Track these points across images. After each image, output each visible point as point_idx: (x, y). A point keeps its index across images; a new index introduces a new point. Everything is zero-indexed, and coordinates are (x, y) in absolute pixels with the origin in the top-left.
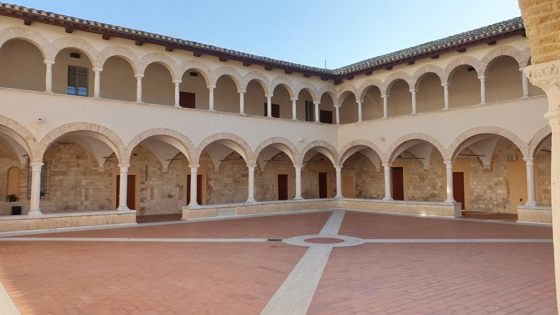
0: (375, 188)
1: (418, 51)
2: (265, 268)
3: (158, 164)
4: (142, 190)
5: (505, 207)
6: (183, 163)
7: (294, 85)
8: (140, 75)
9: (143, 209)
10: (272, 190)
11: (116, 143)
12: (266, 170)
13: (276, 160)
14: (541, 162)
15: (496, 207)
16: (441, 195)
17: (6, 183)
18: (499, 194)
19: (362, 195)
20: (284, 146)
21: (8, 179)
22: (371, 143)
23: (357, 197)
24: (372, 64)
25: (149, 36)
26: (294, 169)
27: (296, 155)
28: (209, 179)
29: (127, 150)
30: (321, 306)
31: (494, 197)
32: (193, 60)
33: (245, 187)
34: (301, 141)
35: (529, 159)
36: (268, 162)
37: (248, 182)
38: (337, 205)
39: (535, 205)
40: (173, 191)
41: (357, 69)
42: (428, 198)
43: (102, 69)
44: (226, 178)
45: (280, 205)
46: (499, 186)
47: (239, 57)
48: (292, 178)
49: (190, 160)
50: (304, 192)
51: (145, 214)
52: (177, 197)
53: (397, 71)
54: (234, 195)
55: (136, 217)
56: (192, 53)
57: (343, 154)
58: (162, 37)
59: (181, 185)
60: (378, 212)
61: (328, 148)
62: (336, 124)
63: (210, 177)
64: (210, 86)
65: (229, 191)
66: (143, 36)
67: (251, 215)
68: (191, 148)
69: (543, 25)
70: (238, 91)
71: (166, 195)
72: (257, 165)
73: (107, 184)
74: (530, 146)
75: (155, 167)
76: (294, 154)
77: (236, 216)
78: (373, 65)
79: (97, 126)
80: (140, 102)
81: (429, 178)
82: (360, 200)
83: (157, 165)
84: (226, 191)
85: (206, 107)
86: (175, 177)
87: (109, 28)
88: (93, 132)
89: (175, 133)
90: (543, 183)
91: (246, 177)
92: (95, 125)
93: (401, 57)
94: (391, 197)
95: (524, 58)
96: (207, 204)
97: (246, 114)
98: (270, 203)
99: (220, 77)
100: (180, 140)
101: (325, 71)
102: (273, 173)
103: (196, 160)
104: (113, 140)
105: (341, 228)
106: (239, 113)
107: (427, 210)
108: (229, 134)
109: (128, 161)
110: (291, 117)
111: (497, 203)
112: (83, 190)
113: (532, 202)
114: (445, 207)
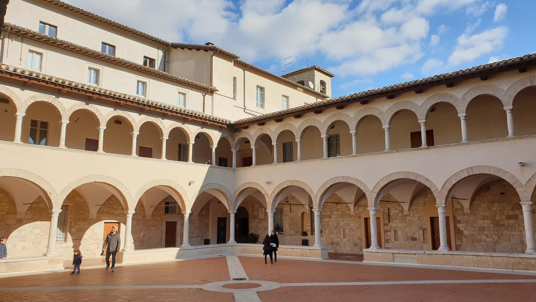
4: (386, 231)
28: (456, 222)
32: (365, 109)
40: (416, 233)
45: (484, 259)
59: (424, 228)
63: (458, 219)
71: (410, 237)
73: (358, 225)
79: (297, 181)
83: (398, 208)
84: (482, 236)
96: (457, 249)
98: (463, 254)
112: (342, 230)
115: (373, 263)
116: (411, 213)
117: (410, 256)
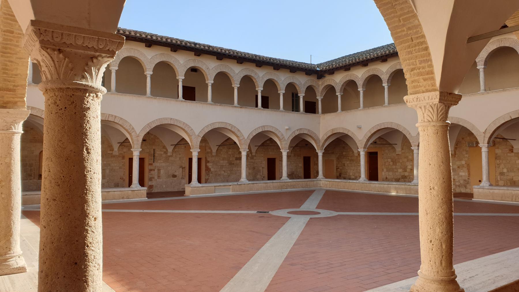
0: (353, 170)
1: (390, 50)
2: (254, 232)
3: (164, 148)
4: (151, 170)
5: (466, 187)
6: (185, 147)
7: (281, 80)
8: (149, 73)
9: (151, 187)
10: (262, 172)
11: (129, 131)
12: (257, 154)
13: (265, 146)
14: (498, 148)
15: (458, 187)
16: (410, 177)
17: (38, 164)
18: (461, 176)
19: (342, 176)
20: (271, 133)
21: (39, 161)
22: (349, 131)
23: (338, 178)
24: (351, 61)
25: (157, 40)
26: (281, 153)
27: (283, 141)
28: (207, 162)
29: (139, 136)
30: (295, 257)
31: (457, 178)
33: (238, 169)
34: (287, 129)
35: (484, 145)
36: (258, 147)
37: (241, 164)
38: (318, 185)
39: (488, 185)
40: (177, 171)
41: (337, 66)
42: (400, 179)
43: (118, 68)
44: (222, 160)
45: (269, 184)
46: (462, 169)
47: (234, 56)
48: (280, 161)
49: (191, 145)
50: (290, 174)
51: (153, 191)
52: (180, 177)
53: (372, 68)
54: (229, 176)
55: (147, 193)
56: (193, 53)
57: (324, 140)
58: (168, 40)
59: (183, 167)
60: (354, 191)
61: (311, 135)
62: (318, 114)
63: (208, 160)
64: (209, 81)
65: (224, 172)
66: (152, 40)
67: (244, 192)
68: (192, 135)
69: (412, 73)
70: (233, 86)
72: (248, 150)
74: (485, 135)
75: (161, 151)
76: (281, 140)
77: (231, 193)
78: (351, 62)
80: (150, 96)
81: (401, 161)
82: (339, 181)
83: (163, 149)
85: (205, 100)
86: (178, 159)
87: (123, 33)
88: (110, 121)
89: (179, 122)
90: (499, 167)
91: (239, 160)
92: (112, 116)
93: (375, 55)
94: (366, 178)
95: (482, 57)
96: (206, 183)
97: (239, 106)
99: (217, 74)
100: (183, 128)
101: (309, 67)
102: (262, 156)
103: (196, 145)
104: (127, 128)
105: (319, 203)
106: (234, 105)
107: (396, 189)
108: (225, 123)
109: (140, 146)
110: (278, 108)
111: (459, 184)
113: (486, 183)
114: (412, 187)
115: (208, 195)
116: (174, 154)
117: (221, 187)
